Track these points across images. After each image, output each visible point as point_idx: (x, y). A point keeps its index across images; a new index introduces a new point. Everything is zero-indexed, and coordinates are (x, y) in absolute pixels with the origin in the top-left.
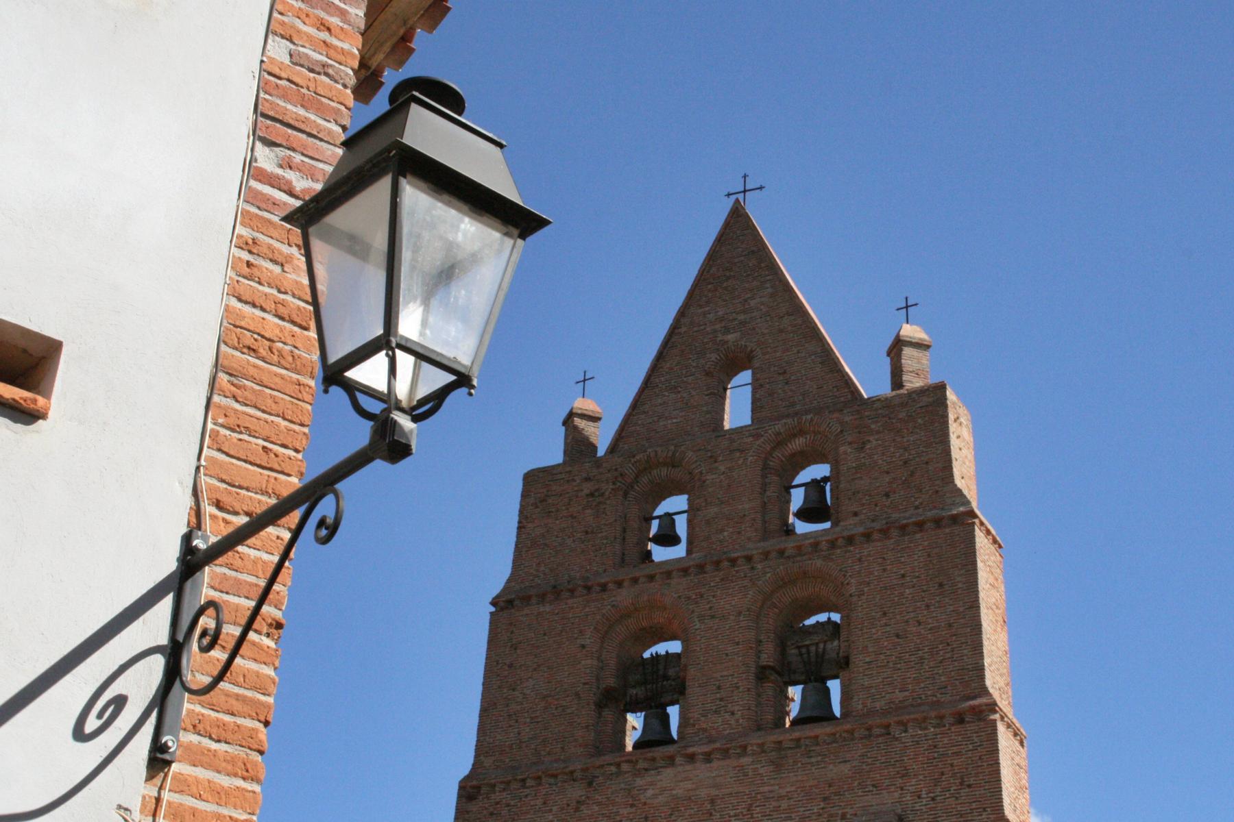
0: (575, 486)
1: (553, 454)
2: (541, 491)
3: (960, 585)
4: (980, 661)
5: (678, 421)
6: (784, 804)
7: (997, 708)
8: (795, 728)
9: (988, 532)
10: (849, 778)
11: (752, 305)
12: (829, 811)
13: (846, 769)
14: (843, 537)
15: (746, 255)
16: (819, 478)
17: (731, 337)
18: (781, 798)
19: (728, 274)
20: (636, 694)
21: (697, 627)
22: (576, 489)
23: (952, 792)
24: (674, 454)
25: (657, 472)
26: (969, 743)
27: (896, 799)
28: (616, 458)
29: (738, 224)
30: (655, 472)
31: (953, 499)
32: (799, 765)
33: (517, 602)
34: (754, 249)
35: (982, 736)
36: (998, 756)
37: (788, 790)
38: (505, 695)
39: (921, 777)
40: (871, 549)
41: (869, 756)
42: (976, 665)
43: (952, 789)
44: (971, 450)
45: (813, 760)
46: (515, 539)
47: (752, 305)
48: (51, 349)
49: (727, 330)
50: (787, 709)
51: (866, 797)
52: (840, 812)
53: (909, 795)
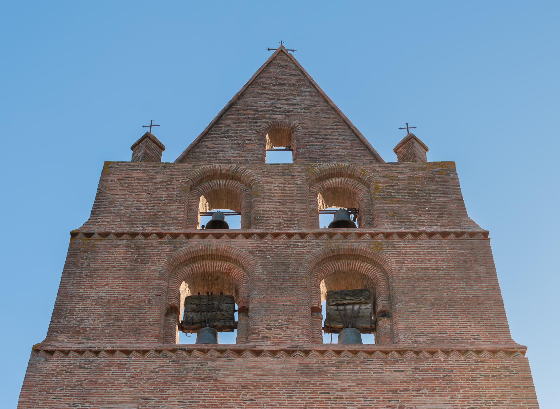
3: (482, 275)
6: (345, 395)
12: (387, 403)
17: (279, 117)
18: (344, 390)
19: (274, 83)
20: (192, 317)
21: (260, 271)
23: (495, 402)
25: (217, 182)
26: (506, 370)
27: (447, 401)
32: (359, 369)
35: (517, 367)
37: (350, 385)
38: (81, 294)
39: (467, 389)
41: (420, 370)
42: (435, 400)
43: (495, 399)
45: (371, 366)
49: (274, 112)
51: (420, 397)
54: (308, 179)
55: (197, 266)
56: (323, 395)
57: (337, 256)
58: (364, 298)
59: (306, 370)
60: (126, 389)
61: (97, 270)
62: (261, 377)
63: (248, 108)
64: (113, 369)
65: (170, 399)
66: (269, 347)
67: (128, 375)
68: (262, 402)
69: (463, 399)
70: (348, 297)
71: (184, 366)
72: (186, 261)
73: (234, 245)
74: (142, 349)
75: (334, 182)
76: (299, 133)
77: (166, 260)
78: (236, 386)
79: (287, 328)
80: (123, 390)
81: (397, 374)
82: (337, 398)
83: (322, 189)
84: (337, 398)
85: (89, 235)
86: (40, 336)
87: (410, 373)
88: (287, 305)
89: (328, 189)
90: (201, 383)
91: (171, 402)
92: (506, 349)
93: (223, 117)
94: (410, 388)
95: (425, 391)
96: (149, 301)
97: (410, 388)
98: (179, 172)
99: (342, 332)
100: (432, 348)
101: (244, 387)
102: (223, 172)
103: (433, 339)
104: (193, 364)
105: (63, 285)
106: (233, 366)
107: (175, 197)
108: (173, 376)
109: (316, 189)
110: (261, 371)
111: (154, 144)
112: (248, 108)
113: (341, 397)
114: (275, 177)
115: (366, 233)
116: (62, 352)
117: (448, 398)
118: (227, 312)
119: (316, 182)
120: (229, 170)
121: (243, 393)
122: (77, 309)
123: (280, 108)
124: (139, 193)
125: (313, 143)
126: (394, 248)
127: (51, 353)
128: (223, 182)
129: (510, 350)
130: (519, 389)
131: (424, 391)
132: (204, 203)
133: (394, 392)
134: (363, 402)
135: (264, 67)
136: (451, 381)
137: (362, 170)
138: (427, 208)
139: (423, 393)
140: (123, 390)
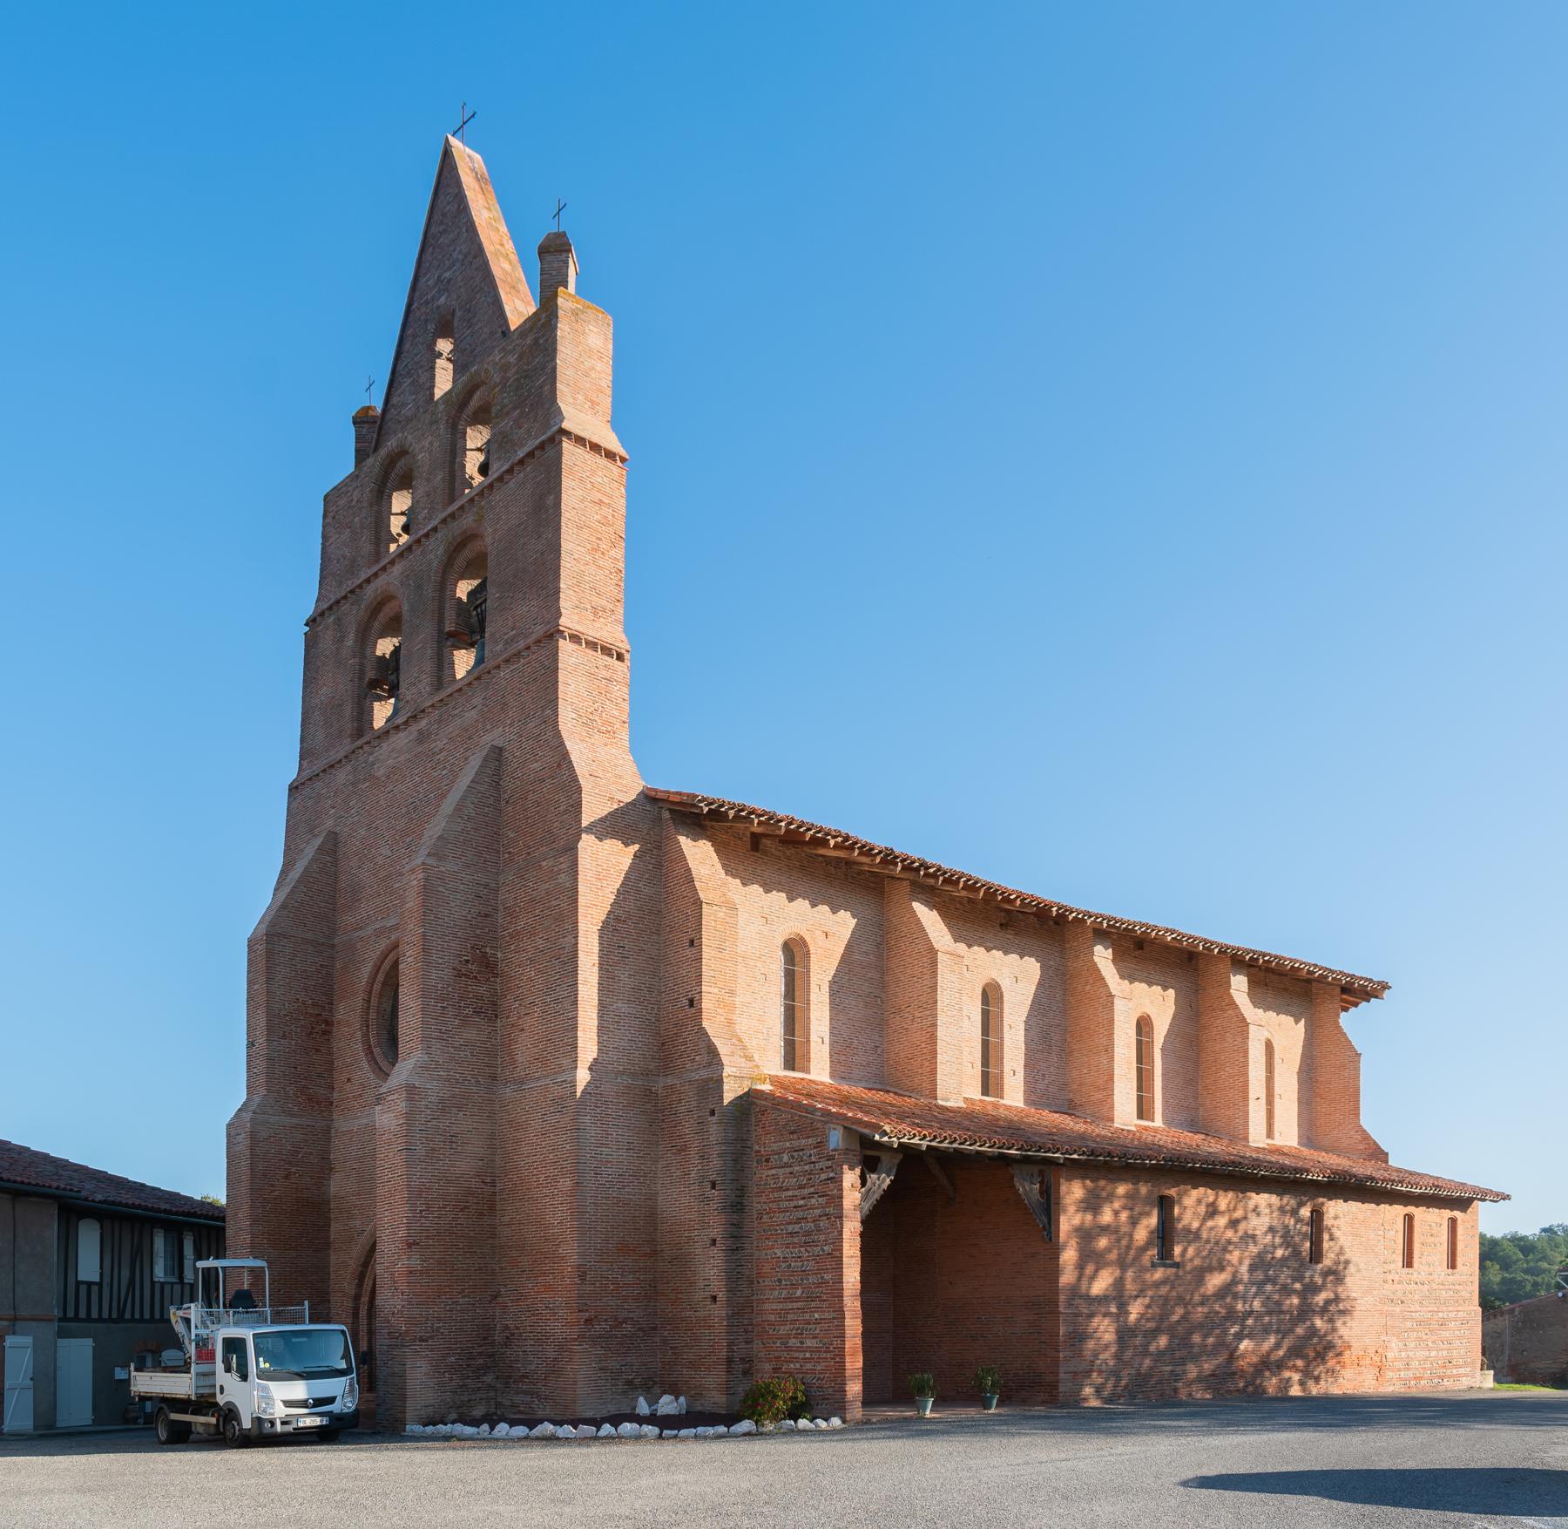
7: (561, 628)
72: (370, 618)
89: (475, 413)
103: (507, 643)
108: (352, 784)
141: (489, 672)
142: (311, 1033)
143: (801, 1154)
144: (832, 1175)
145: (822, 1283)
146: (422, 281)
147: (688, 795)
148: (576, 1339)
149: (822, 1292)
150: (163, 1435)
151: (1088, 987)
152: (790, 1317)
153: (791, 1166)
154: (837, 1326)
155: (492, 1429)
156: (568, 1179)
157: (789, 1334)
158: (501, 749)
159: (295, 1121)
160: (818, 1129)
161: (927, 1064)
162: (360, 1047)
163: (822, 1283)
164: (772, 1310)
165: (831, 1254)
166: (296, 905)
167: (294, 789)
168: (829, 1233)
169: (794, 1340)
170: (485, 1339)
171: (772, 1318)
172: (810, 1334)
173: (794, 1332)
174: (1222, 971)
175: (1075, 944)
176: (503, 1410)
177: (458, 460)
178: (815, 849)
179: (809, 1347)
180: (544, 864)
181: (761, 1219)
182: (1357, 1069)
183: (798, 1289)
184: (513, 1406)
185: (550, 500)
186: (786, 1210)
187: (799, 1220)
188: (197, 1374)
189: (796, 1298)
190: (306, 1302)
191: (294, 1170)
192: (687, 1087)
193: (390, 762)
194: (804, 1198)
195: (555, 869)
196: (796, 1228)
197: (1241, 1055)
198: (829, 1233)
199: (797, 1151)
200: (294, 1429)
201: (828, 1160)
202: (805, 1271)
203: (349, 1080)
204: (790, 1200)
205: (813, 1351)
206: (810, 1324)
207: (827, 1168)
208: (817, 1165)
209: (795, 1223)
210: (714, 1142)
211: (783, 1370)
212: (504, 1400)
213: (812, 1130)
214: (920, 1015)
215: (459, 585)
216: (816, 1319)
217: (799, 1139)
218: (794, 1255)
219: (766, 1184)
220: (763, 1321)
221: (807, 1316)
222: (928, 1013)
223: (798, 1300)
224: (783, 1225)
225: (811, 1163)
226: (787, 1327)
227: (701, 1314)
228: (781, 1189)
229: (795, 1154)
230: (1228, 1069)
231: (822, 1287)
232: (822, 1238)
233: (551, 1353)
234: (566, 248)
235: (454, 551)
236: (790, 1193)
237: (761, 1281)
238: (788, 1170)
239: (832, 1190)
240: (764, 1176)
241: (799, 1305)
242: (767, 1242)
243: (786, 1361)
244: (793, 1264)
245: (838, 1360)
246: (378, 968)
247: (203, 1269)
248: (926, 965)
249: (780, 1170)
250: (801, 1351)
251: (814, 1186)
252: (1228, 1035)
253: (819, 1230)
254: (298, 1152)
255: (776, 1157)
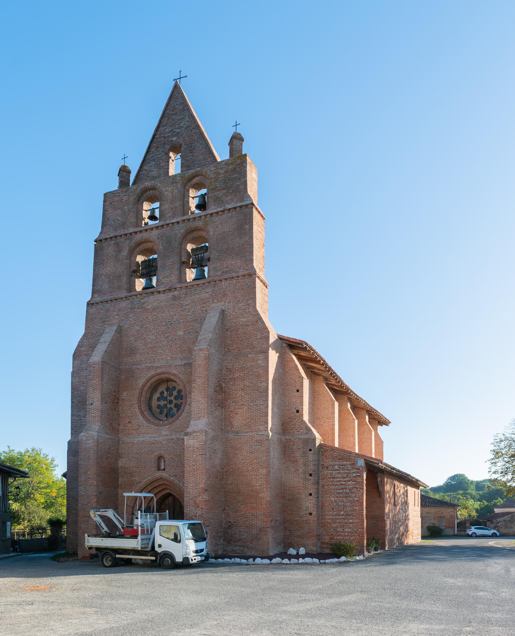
0: (121, 198)
1: (114, 185)
2: (110, 200)
4: (252, 257)
5: (156, 172)
6: (187, 307)
7: (257, 274)
8: (193, 281)
9: (259, 212)
10: (208, 298)
11: (181, 125)
13: (207, 295)
14: (209, 214)
15: (179, 105)
16: (203, 194)
17: (174, 139)
18: (187, 305)
20: (143, 272)
21: (161, 248)
22: (121, 199)
24: (154, 185)
28: (134, 187)
29: (176, 88)
30: (148, 192)
31: (247, 199)
32: (193, 294)
33: (103, 241)
34: (182, 102)
36: (256, 290)
39: (231, 297)
40: (218, 218)
44: (256, 182)
45: (197, 292)
46: (102, 218)
47: (181, 125)
48: (390, 422)
49: (173, 136)
50: (466, 477)
52: (205, 309)
53: (227, 303)
54: (183, 184)
55: (141, 247)
56: (180, 309)
57: (192, 231)
58: (204, 251)
59: (174, 298)
60: (117, 317)
61: (104, 259)
62: (159, 304)
63: (161, 136)
64: (112, 308)
65: (130, 319)
66: (162, 289)
67: (117, 310)
68: (159, 315)
69: (229, 303)
70: (198, 251)
71: (134, 303)
72: (136, 246)
73: (152, 235)
74: (120, 297)
75: (196, 180)
76: (184, 146)
77: (127, 249)
78: (151, 310)
79: (170, 277)
80: (116, 317)
81: (206, 294)
82: (184, 310)
83: (191, 186)
84: (184, 310)
85: (101, 241)
86: (89, 297)
87: (211, 293)
88: (170, 265)
89: (194, 185)
90: (140, 310)
91: (131, 320)
92: (248, 274)
93: (151, 146)
94: (210, 300)
95: (215, 301)
96: (123, 272)
97: (210, 300)
98: (132, 193)
99: (197, 268)
100: (220, 279)
101: (154, 310)
102: (149, 188)
103: (223, 272)
104: (137, 301)
105: (94, 270)
106: (149, 300)
107: (131, 209)
108: (130, 308)
109: (188, 187)
110: (159, 301)
111: (125, 173)
112: (161, 136)
113: (185, 309)
114: (169, 186)
115: (202, 216)
116: (96, 303)
117: (223, 303)
118: (155, 267)
119: (188, 183)
120: (151, 186)
121: (153, 312)
122: (99, 281)
123: (175, 131)
124: (118, 210)
125: (188, 154)
126: (213, 222)
127: (93, 304)
128: (151, 192)
129: (250, 274)
130: (250, 294)
131: (215, 301)
132: (148, 203)
133: (204, 303)
134: (193, 310)
135: (168, 102)
136: (225, 294)
137: (205, 172)
138: (230, 192)
139: (214, 302)
140: (116, 317)
141: (215, 281)
142: (113, 402)
143: (344, 467)
144: (358, 475)
145: (354, 510)
146: (162, 129)
147: (300, 340)
148: (269, 527)
149: (353, 513)
150: (107, 563)
151: (345, 416)
152: (338, 521)
153: (339, 470)
154: (360, 525)
155: (254, 560)
156: (265, 470)
157: (338, 527)
158: (224, 310)
159: (109, 436)
160: (352, 459)
161: (331, 437)
162: (137, 410)
163: (354, 510)
164: (329, 518)
165: (358, 501)
166: (109, 351)
167: (90, 304)
168: (357, 494)
169: (340, 529)
170: (221, 526)
171: (329, 521)
172: (348, 527)
173: (340, 526)
174: (363, 414)
175: (341, 401)
176: (227, 552)
177: (185, 199)
178: (307, 362)
179: (347, 531)
180: (250, 355)
181: (323, 487)
182: (383, 446)
183: (342, 511)
184: (233, 550)
185: (247, 227)
186: (336, 485)
187: (342, 489)
188: (142, 540)
189: (341, 515)
190: (167, 511)
191: (109, 456)
192: (298, 440)
193: (155, 304)
194: (345, 482)
195: (256, 358)
196: (341, 491)
197: (370, 440)
198: (357, 494)
199: (342, 465)
200: (197, 562)
201: (357, 470)
202: (345, 506)
203: (129, 422)
204: (339, 482)
205: (349, 533)
206: (348, 523)
207: (356, 472)
208: (351, 471)
209: (340, 490)
210: (311, 460)
211: (335, 539)
212: (227, 549)
213: (349, 459)
214: (327, 421)
215: (188, 245)
216: (351, 522)
217: (343, 461)
218: (340, 500)
219: (327, 476)
220: (324, 522)
221: (346, 521)
222: (331, 420)
223: (342, 515)
224: (335, 490)
225: (348, 470)
226: (336, 525)
227: (305, 519)
228: (334, 478)
229: (341, 467)
230: (365, 444)
231: (353, 511)
232: (354, 495)
233: (254, 532)
234: (243, 139)
235: (189, 233)
236: (338, 479)
237: (324, 508)
238: (338, 472)
239: (359, 480)
240: (326, 473)
241: (343, 517)
242: (327, 495)
243: (336, 536)
244: (339, 503)
245: (361, 536)
246: (148, 381)
247: (127, 496)
248: (330, 405)
249: (333, 471)
250: (344, 533)
251: (350, 478)
252: (365, 433)
253: (352, 493)
254: (110, 449)
255: (332, 467)
